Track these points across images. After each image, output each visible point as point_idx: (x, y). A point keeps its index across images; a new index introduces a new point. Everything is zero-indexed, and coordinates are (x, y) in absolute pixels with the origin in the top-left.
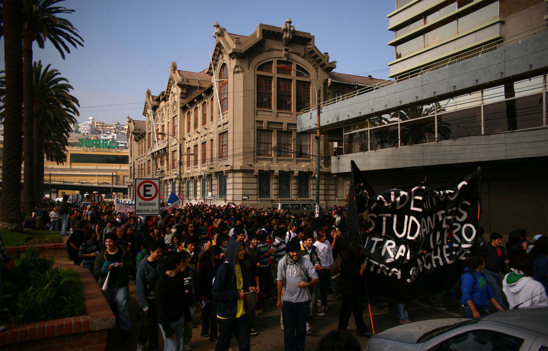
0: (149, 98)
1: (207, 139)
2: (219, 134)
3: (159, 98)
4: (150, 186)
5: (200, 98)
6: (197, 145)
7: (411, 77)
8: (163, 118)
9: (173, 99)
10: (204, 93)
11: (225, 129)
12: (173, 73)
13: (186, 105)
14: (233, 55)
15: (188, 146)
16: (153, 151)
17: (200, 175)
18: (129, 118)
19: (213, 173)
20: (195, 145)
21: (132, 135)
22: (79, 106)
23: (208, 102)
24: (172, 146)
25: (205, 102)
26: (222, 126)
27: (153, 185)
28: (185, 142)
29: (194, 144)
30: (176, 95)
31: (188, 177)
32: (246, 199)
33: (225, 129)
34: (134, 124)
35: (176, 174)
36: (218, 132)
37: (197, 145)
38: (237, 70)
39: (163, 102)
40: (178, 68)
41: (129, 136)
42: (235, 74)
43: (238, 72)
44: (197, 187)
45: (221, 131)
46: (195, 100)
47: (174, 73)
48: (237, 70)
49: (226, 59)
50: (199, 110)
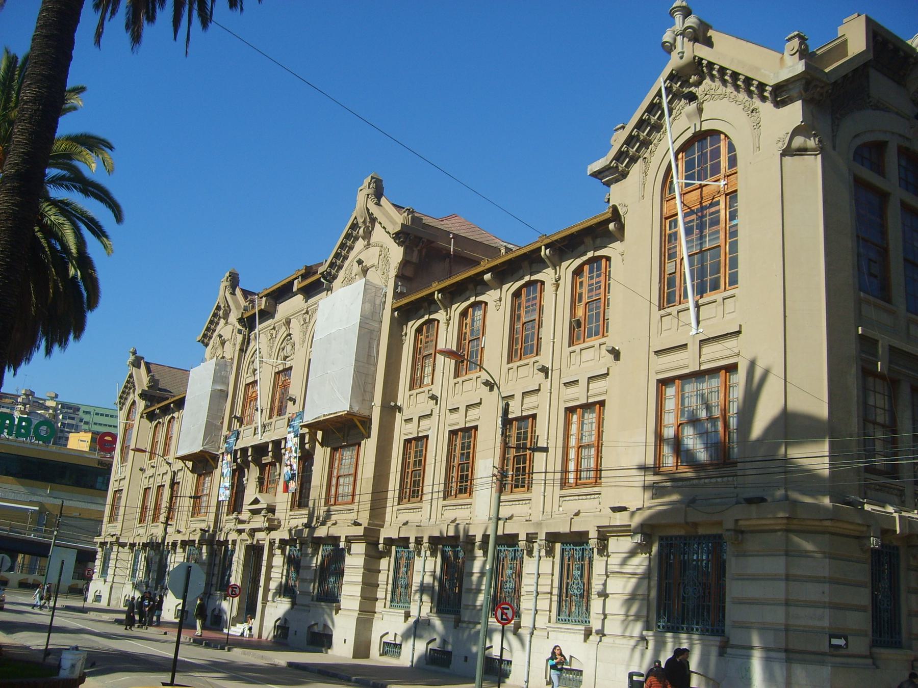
0: (233, 293)
1: (154, 484)
2: (405, 440)
3: (291, 284)
4: (508, 609)
5: (453, 294)
6: (122, 490)
7: (535, 427)
8: (289, 347)
9: (219, 352)
10: (439, 291)
11: (470, 421)
12: (231, 293)
13: (539, 249)
14: (143, 395)
15: (117, 486)
16: (241, 444)
17: (145, 542)
18: (134, 353)
19: (179, 542)
20: (159, 484)
21: (134, 403)
22: (109, 20)
23: (163, 424)
24: (116, 481)
25: (173, 418)
26: (416, 420)
27: (510, 609)
28: (144, 476)
29: (159, 483)
30: (227, 343)
31: (139, 543)
32: (839, 646)
33: (470, 421)
34: (149, 371)
35: (356, 524)
36: (405, 435)
37: (122, 490)
38: (799, 141)
39: (300, 297)
40: (244, 284)
41: (126, 399)
42: (787, 159)
43: (802, 151)
44: (109, 560)
45: (458, 424)
46: (172, 405)
47: (378, 204)
48: (799, 141)
49: (135, 396)
50: (175, 422)
